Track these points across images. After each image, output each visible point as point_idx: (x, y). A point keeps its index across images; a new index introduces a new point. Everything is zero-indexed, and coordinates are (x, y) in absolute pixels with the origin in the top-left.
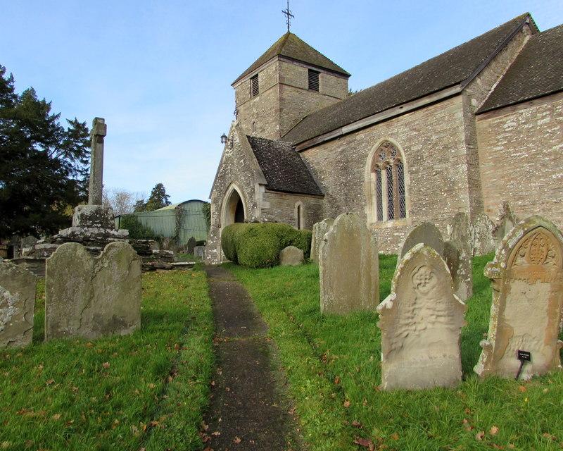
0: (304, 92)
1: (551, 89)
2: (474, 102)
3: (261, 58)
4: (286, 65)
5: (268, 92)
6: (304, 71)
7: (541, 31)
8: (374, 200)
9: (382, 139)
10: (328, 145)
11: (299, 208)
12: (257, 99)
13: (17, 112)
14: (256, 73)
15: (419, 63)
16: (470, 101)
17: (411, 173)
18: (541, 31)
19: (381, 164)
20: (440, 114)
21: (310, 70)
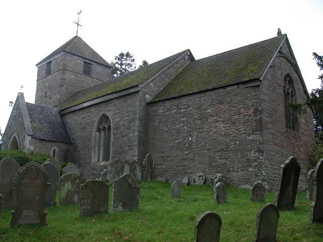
0: (79, 75)
1: (228, 93)
2: (147, 96)
3: (48, 57)
4: (68, 57)
5: (56, 73)
6: (81, 62)
7: (196, 59)
8: (97, 149)
9: (103, 113)
10: (77, 113)
11: (54, 151)
12: (49, 77)
13: (185, 176)
14: (50, 60)
15: (36, 85)
16: (145, 96)
17: (115, 134)
18: (196, 59)
19: (101, 128)
20: (129, 101)
21: (84, 62)
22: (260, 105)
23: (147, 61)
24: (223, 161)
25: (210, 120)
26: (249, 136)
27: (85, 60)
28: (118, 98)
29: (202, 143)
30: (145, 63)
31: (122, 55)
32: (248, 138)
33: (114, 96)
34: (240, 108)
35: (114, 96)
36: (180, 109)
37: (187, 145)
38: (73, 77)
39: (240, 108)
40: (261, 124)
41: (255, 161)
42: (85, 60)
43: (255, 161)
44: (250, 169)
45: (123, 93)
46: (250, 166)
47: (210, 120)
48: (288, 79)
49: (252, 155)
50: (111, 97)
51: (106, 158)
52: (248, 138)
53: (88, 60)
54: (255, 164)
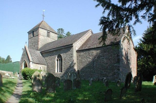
0: (45, 37)
6: (46, 32)
22: (119, 53)
23: (99, 22)
24: (105, 73)
25: (101, 58)
26: (115, 64)
27: (48, 31)
28: (66, 48)
29: (98, 66)
30: (9, 58)
31: (60, 29)
32: (115, 65)
33: (63, 47)
34: (112, 54)
35: (63, 47)
36: (89, 53)
37: (92, 67)
38: (43, 38)
39: (112, 54)
40: (119, 60)
41: (117, 73)
42: (48, 31)
43: (117, 73)
44: (115, 76)
45: (65, 47)
46: (115, 75)
47: (101, 58)
48: (128, 43)
49: (116, 71)
50: (62, 48)
51: (61, 71)
52: (115, 65)
53: (49, 31)
54: (116, 74)
